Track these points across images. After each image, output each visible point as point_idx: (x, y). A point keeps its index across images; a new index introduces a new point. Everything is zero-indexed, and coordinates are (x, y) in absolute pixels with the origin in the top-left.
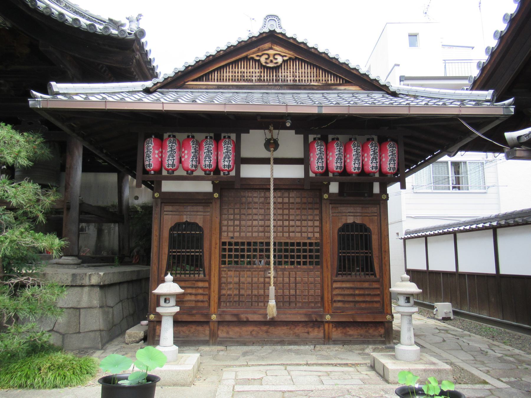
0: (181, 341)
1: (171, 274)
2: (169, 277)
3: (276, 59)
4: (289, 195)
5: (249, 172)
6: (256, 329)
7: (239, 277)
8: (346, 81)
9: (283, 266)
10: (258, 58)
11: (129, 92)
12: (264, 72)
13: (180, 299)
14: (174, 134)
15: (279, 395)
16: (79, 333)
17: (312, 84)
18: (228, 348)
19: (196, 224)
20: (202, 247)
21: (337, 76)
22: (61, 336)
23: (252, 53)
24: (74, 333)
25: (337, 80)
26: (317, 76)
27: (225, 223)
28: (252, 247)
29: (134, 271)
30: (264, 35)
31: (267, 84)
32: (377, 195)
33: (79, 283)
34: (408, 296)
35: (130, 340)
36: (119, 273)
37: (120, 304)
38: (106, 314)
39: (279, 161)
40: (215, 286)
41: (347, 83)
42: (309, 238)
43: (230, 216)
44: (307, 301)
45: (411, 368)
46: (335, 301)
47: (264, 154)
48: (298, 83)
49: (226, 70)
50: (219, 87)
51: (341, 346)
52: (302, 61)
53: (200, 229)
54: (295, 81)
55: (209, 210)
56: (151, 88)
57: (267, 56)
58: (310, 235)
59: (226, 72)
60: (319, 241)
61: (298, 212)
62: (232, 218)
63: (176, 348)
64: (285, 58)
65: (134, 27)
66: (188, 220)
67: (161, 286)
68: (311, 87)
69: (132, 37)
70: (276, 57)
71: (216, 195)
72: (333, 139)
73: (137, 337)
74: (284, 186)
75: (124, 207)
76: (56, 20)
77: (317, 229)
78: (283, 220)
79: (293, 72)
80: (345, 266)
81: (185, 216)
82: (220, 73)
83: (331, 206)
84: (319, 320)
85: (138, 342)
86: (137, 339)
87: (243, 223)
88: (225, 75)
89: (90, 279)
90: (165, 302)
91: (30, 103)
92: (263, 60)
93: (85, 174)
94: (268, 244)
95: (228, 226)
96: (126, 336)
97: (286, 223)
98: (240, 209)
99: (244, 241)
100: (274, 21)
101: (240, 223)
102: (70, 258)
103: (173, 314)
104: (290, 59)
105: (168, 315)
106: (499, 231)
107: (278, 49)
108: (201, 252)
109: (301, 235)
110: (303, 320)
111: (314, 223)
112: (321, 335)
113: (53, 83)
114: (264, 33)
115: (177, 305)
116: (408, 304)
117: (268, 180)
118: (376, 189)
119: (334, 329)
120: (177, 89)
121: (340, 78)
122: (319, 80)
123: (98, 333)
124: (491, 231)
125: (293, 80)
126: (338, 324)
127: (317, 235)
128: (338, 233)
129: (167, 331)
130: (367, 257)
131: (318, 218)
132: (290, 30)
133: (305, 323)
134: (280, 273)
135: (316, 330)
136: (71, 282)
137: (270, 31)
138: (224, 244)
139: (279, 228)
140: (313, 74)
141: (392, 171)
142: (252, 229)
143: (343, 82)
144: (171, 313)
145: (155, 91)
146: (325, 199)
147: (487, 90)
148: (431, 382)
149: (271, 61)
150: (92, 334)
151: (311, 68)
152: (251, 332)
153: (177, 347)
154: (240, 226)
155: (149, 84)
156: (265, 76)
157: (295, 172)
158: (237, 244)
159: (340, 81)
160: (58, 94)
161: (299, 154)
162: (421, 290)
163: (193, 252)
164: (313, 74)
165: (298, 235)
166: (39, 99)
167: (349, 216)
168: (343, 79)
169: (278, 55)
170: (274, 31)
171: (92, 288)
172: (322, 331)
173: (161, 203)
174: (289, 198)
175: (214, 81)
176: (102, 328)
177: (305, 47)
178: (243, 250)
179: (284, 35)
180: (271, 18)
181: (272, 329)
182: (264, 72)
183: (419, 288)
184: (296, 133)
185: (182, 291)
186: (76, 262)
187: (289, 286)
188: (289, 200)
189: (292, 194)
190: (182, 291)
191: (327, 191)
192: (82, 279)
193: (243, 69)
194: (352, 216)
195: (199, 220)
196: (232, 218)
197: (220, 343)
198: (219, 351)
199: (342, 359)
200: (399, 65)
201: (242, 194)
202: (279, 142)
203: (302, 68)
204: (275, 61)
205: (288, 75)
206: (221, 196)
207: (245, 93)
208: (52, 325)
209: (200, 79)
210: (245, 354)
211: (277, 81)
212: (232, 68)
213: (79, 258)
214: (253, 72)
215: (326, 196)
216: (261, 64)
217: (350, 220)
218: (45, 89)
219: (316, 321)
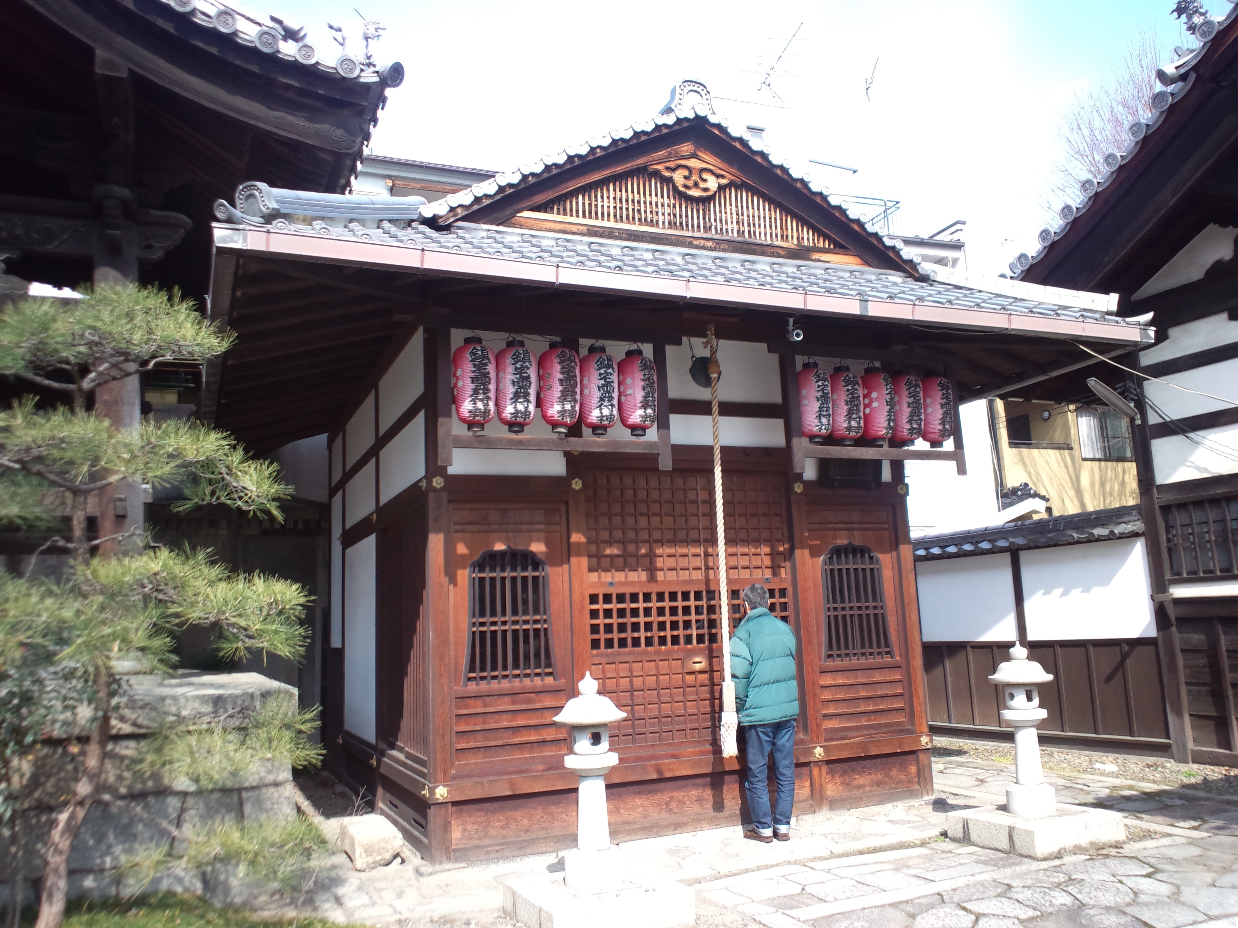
2: (588, 685)
3: (705, 181)
10: (667, 174)
12: (680, 207)
14: (518, 337)
15: (898, 917)
23: (656, 159)
31: (690, 234)
32: (887, 484)
35: (370, 859)
41: (839, 248)
49: (602, 193)
56: (441, 217)
57: (686, 173)
59: (602, 197)
64: (724, 182)
68: (774, 250)
70: (705, 176)
71: (577, 484)
72: (806, 366)
73: (387, 851)
82: (590, 199)
88: (600, 204)
92: (678, 177)
94: (712, 594)
103: (606, 772)
106: (1024, 556)
107: (709, 160)
118: (886, 475)
119: (828, 778)
124: (1007, 557)
130: (876, 615)
141: (853, 434)
147: (1107, 292)
149: (696, 185)
156: (684, 212)
162: (1050, 677)
163: (526, 622)
167: (840, 529)
172: (808, 784)
175: (609, 220)
177: (765, 164)
180: (695, 88)
182: (680, 207)
183: (1047, 671)
184: (770, 350)
190: (624, 715)
194: (844, 529)
211: (707, 229)
212: (614, 190)
214: (657, 202)
216: (675, 188)
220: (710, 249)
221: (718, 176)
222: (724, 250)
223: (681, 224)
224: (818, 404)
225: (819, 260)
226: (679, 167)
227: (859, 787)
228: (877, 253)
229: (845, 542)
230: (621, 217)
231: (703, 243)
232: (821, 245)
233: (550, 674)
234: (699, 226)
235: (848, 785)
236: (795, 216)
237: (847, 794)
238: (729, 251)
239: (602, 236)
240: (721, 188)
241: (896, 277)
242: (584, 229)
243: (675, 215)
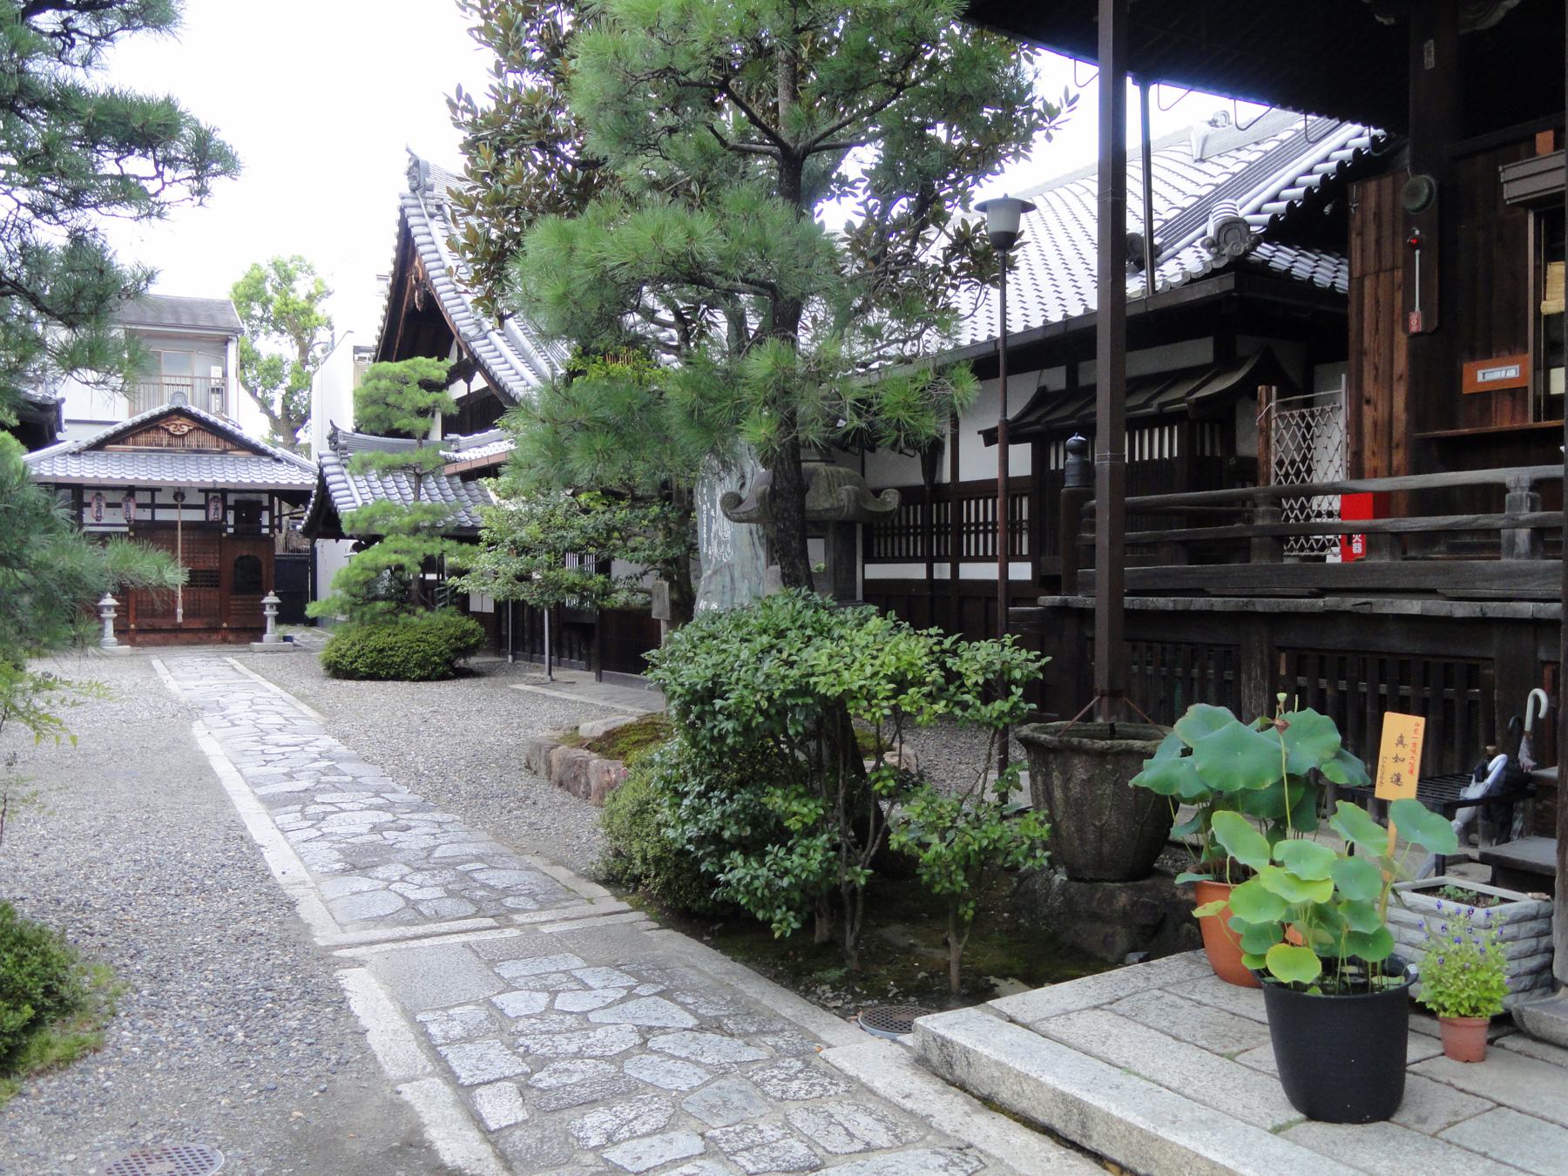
13: (117, 609)
74: (188, 526)
80: (238, 589)
92: (171, 429)
93: (1371, 496)
107: (183, 420)
126: (231, 630)
133: (205, 630)
148: (363, 554)
156: (174, 441)
157: (198, 516)
161: (202, 502)
193: (153, 435)
205: (193, 441)
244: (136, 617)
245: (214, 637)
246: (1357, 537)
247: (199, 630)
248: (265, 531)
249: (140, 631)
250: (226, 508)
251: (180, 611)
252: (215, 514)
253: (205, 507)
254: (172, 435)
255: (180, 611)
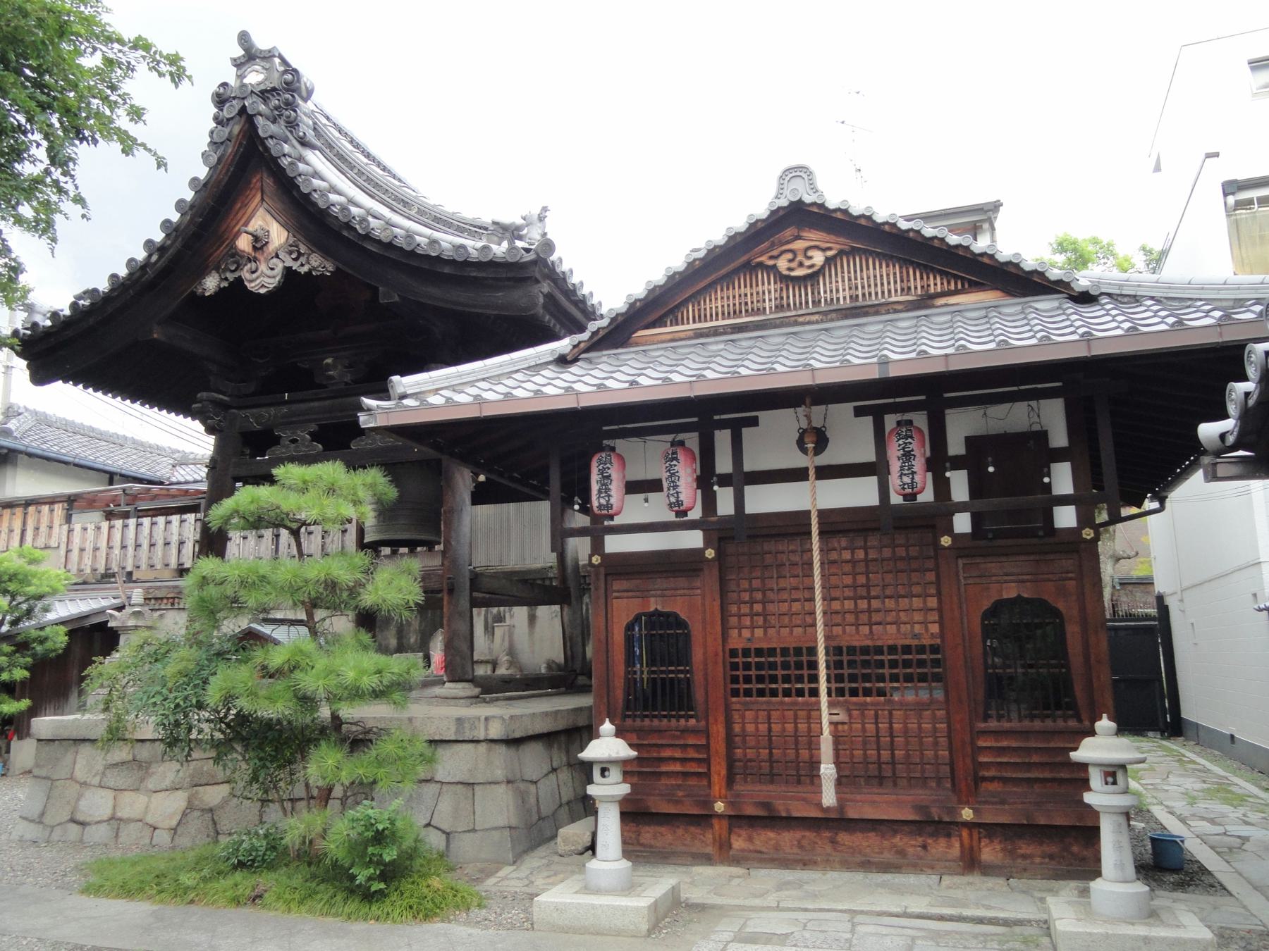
0: (633, 850)
1: (612, 722)
3: (811, 258)
4: (866, 542)
5: (766, 500)
6: (807, 834)
7: (769, 723)
8: (970, 282)
9: (861, 699)
10: (771, 263)
11: (528, 368)
13: (629, 770)
16: (474, 830)
17: (893, 299)
18: (753, 872)
19: (676, 616)
20: (688, 662)
21: (947, 274)
22: (444, 836)
24: (469, 831)
25: (949, 283)
26: (902, 281)
27: (734, 609)
28: (792, 659)
29: (580, 709)
30: (781, 213)
31: (794, 313)
33: (468, 736)
34: (1110, 769)
35: (567, 848)
36: (546, 714)
37: (553, 777)
38: (522, 797)
39: (825, 473)
40: (719, 745)
41: (975, 286)
42: (915, 636)
43: (743, 594)
44: (918, 775)
45: (1110, 932)
46: (984, 779)
47: (798, 460)
48: (861, 302)
50: (699, 334)
51: (1001, 881)
52: (865, 251)
53: (681, 624)
54: (854, 298)
55: (698, 584)
57: (790, 256)
58: (917, 628)
60: (938, 641)
61: (889, 578)
62: (747, 599)
63: (625, 864)
64: (830, 253)
65: (534, 234)
66: (659, 608)
67: (594, 743)
68: (890, 307)
69: (530, 257)
70: (810, 253)
74: (838, 524)
75: (569, 570)
76: (401, 248)
77: (934, 616)
78: (855, 599)
79: (850, 280)
81: (652, 599)
83: (961, 562)
84: (947, 819)
85: (582, 854)
86: (580, 848)
87: (770, 607)
89: (486, 729)
90: (603, 775)
91: (361, 419)
92: (782, 264)
95: (740, 616)
96: (559, 839)
97: (863, 604)
98: (750, 580)
99: (774, 645)
100: (799, 180)
101: (764, 608)
102: (460, 685)
104: (841, 253)
105: (609, 799)
107: (815, 237)
108: (688, 672)
109: (898, 630)
110: (911, 817)
111: (925, 602)
112: (956, 851)
113: (395, 378)
114: (779, 208)
115: (625, 781)
116: (1111, 788)
117: (807, 514)
119: (984, 842)
120: (617, 348)
121: (956, 277)
122: (909, 288)
123: (507, 833)
125: (851, 297)
126: (990, 830)
127: (935, 628)
128: (983, 619)
129: (609, 825)
131: (933, 591)
132: (837, 192)
134: (855, 713)
135: (942, 842)
136: (456, 733)
137: (792, 203)
138: (733, 653)
139: (847, 616)
140: (895, 277)
142: (791, 620)
143: (963, 285)
144: (613, 796)
145: (576, 360)
146: (945, 548)
149: (801, 265)
150: (496, 834)
151: (881, 267)
152: (799, 842)
153: (630, 864)
154: (764, 614)
155: (563, 345)
156: (792, 295)
158: (759, 652)
159: (956, 284)
160: (404, 396)
164: (895, 277)
165: (892, 629)
166: (376, 412)
168: (963, 279)
169: (813, 251)
170: (800, 202)
171: (493, 745)
173: (606, 575)
174: (866, 549)
176: (514, 822)
177: (870, 225)
178: (773, 666)
179: (822, 206)
181: (844, 837)
185: (634, 753)
186: (469, 693)
187: (921, 743)
188: (866, 554)
189: (873, 541)
190: (634, 753)
191: (949, 530)
192: (473, 727)
193: (742, 290)
195: (678, 606)
196: (747, 599)
197: (736, 861)
198: (732, 877)
199: (988, 908)
200: (1216, 155)
201: (766, 547)
202: (828, 434)
203: (868, 269)
204: (808, 263)
206: (720, 553)
207: (750, 338)
208: (429, 815)
209: (653, 325)
210: (781, 887)
213: (476, 686)
214: (768, 290)
215: (946, 541)
216: (780, 273)
217: (1010, 592)
218: (382, 392)
219: (940, 822)
220: (817, 322)
221: (824, 250)
222: (832, 320)
223: (789, 305)
224: (899, 464)
225: (946, 305)
226: (782, 253)
227: (1024, 857)
228: (1020, 282)
229: (1013, 595)
230: (717, 314)
231: (808, 318)
232: (952, 287)
233: (692, 717)
234: (807, 302)
235: (1012, 853)
236: (917, 266)
237: (1008, 861)
238: (838, 319)
239: (707, 336)
240: (828, 261)
241: (1045, 303)
242: (691, 333)
243: (782, 298)
244: (730, 780)
245: (1025, 875)
246: (981, 774)
247: (893, 826)
248: (1066, 517)
249: (737, 820)
250: (938, 463)
251: (827, 770)
252: (910, 480)
253: (876, 469)
254: (786, 280)
255: (827, 770)
